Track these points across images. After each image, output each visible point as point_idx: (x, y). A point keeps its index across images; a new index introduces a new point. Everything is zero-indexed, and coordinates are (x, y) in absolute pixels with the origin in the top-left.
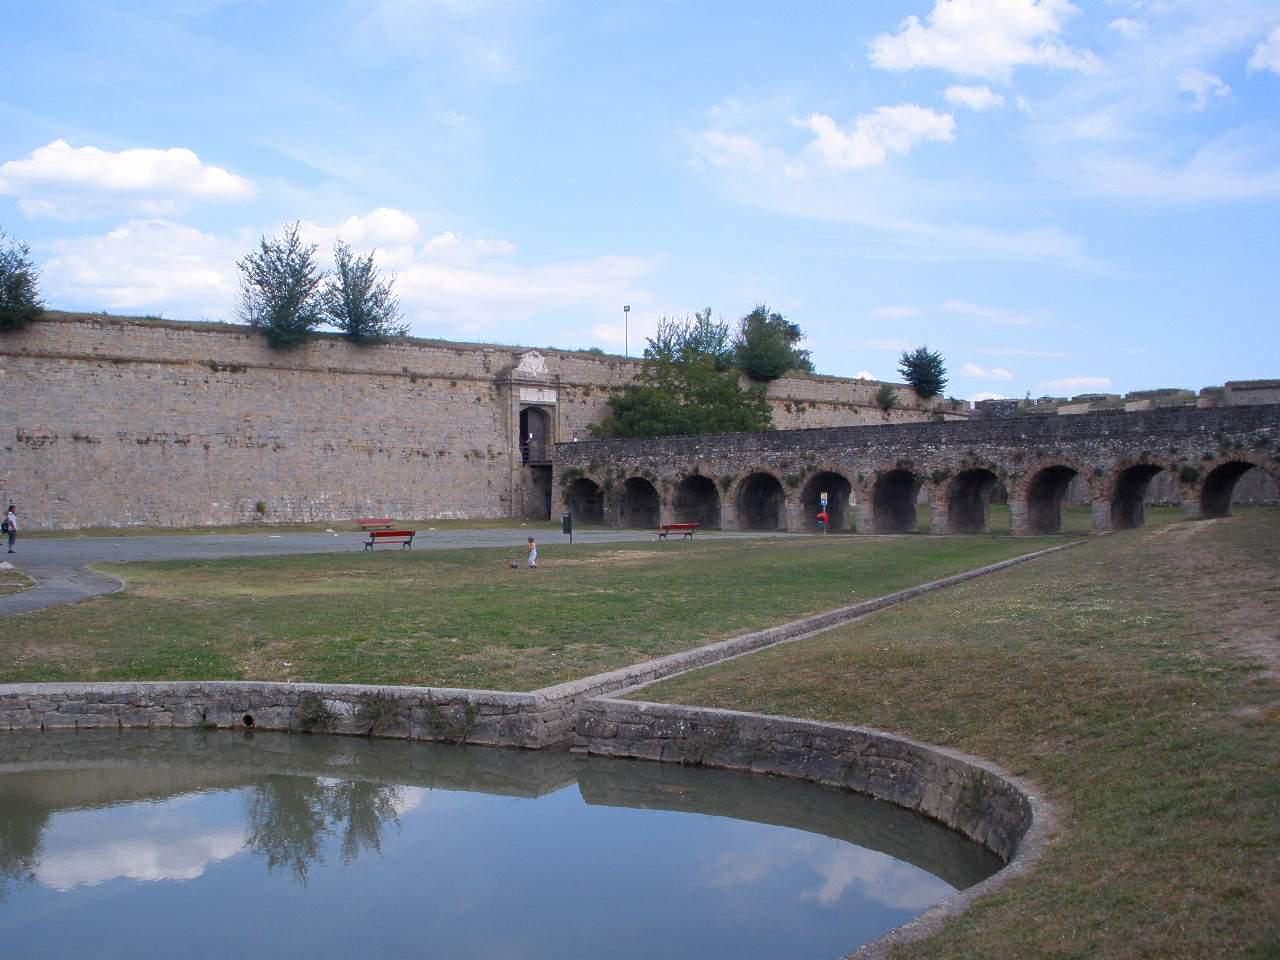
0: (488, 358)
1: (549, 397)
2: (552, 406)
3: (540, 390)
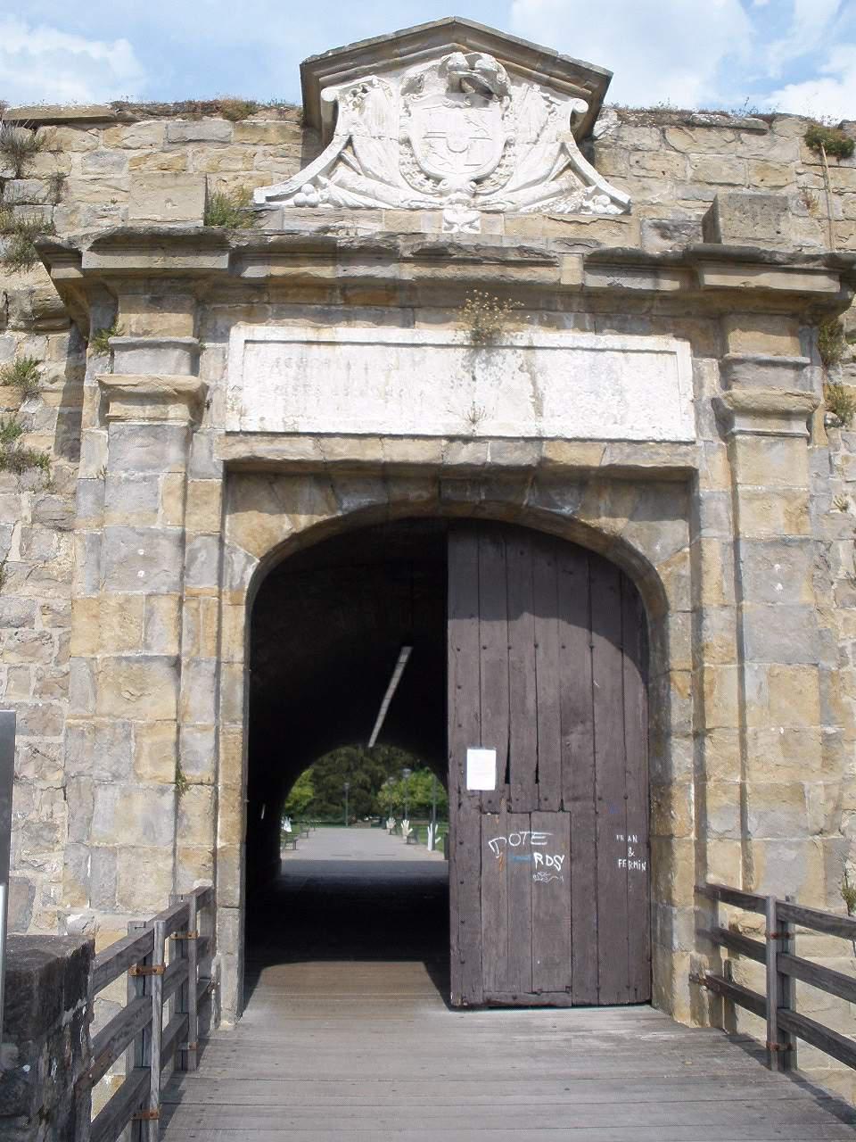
0: (44, 165)
1: (614, 394)
2: (668, 488)
3: (483, 341)
